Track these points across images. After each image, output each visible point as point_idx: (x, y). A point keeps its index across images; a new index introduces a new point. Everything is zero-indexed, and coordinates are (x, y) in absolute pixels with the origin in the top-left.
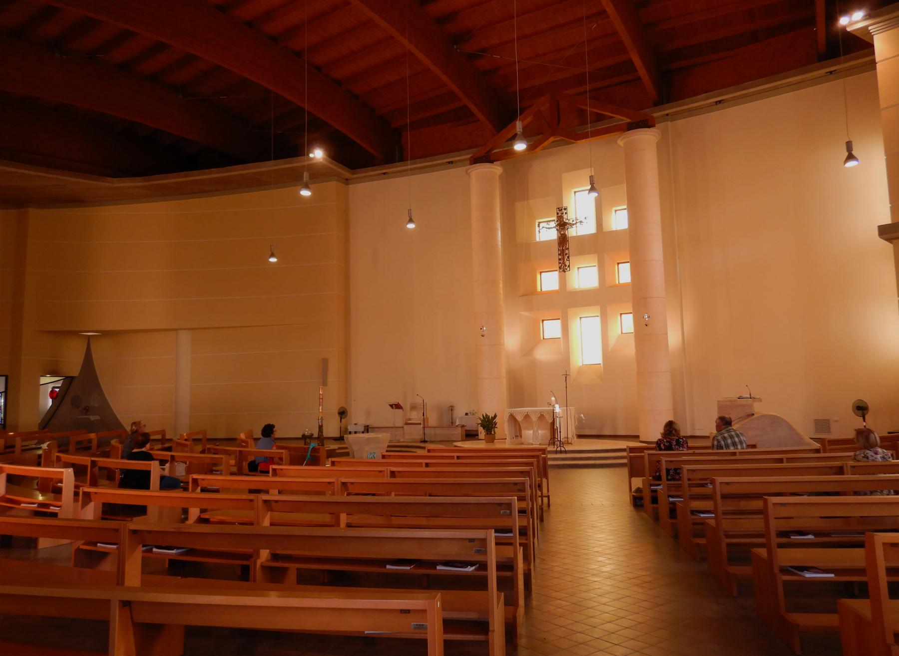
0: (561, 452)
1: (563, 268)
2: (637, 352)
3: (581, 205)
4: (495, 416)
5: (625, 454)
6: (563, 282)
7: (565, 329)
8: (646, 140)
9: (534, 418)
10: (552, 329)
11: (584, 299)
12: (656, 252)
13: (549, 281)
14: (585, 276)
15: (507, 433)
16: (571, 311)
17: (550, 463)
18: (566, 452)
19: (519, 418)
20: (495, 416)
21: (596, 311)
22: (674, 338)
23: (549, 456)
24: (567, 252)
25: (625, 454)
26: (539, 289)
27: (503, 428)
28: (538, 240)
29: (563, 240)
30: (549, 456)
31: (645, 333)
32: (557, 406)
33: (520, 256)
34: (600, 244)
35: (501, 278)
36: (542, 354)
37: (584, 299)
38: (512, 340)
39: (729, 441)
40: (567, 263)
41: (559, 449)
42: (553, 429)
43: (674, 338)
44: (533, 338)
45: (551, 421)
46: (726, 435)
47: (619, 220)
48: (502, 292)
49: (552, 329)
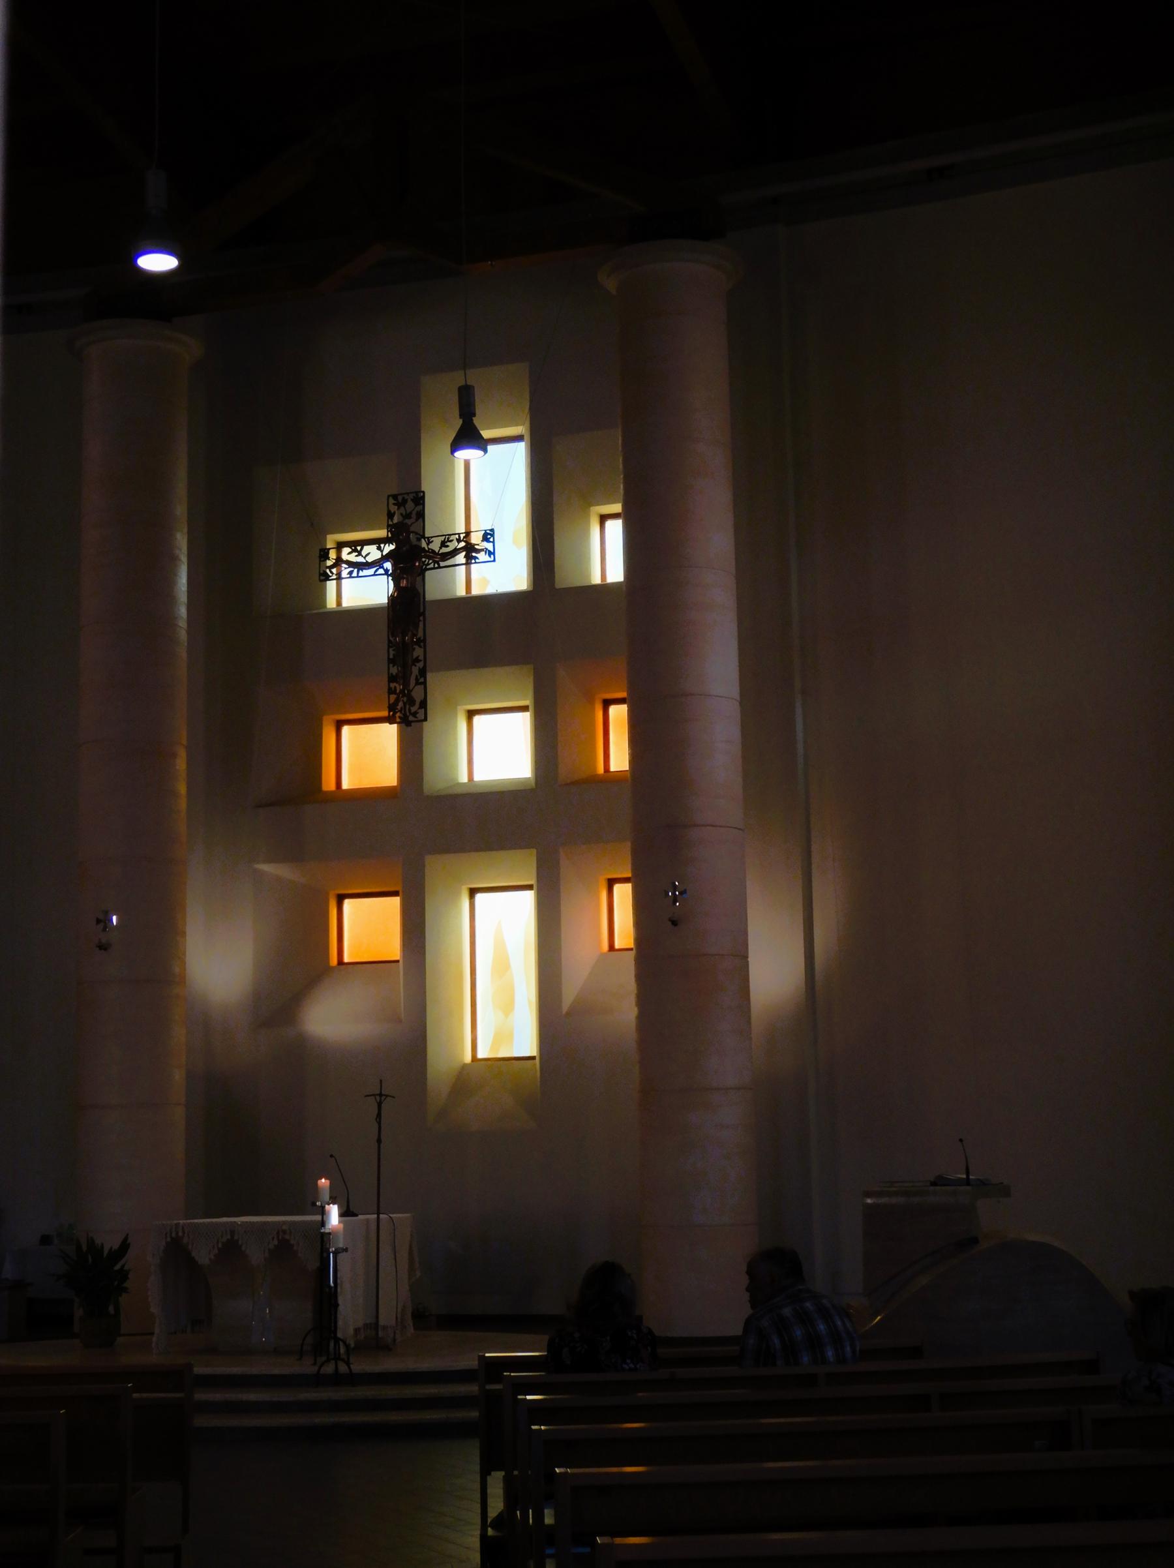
0: (337, 1380)
1: (409, 712)
2: (641, 1017)
3: (489, 490)
4: (125, 1246)
5: (473, 1389)
6: (412, 755)
7: (415, 929)
8: (695, 286)
9: (256, 1255)
10: (367, 926)
11: (488, 826)
12: (717, 668)
13: (366, 755)
14: (496, 747)
15: (154, 1310)
16: (436, 867)
17: (201, 1421)
18: (353, 1379)
19: (203, 1255)
20: (125, 1246)
21: (524, 865)
22: (774, 968)
23: (201, 1396)
24: (418, 652)
25: (473, 1389)
26: (329, 784)
27: (148, 1291)
28: (331, 603)
29: (408, 604)
30: (201, 1396)
31: (679, 954)
32: (334, 1212)
33: (278, 669)
34: (539, 636)
35: (184, 736)
36: (334, 1019)
37: (488, 826)
38: (219, 962)
39: (798, 1333)
40: (417, 693)
41: (329, 1369)
42: (326, 1301)
43: (774, 968)
44: (303, 957)
45: (313, 1265)
46: (787, 1311)
47: (604, 553)
48: (182, 789)
49: (367, 926)
